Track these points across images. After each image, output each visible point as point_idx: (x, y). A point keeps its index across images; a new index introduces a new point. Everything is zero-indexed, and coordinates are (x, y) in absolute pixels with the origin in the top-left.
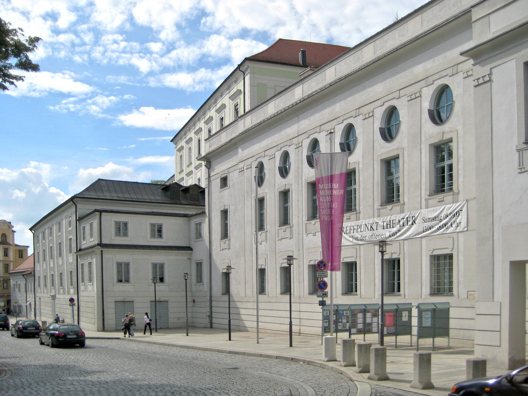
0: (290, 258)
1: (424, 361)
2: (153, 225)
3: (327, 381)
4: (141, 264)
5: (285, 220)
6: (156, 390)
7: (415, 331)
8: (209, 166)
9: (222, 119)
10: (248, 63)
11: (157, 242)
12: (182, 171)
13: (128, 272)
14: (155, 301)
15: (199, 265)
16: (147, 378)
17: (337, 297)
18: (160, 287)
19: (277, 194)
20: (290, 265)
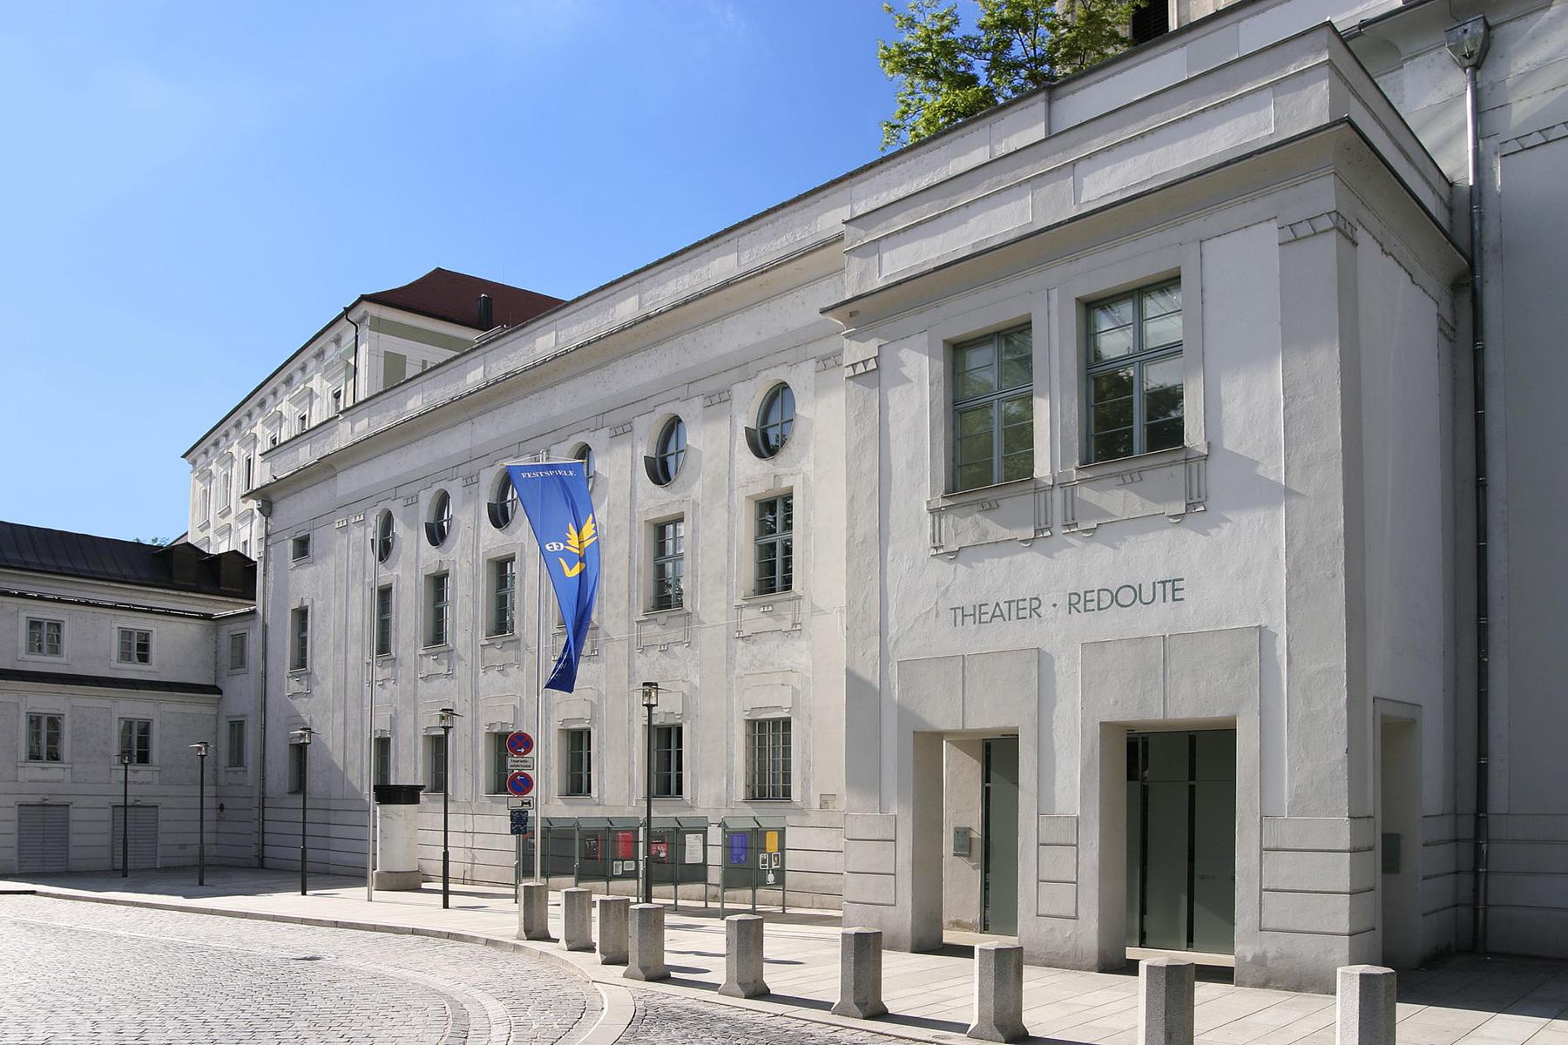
0: (448, 713)
1: (748, 938)
2: (126, 634)
3: (532, 983)
4: (94, 720)
5: (437, 635)
6: (95, 1017)
7: (715, 875)
8: (267, 509)
9: (303, 418)
10: (367, 307)
11: (134, 671)
12: (206, 525)
13: (54, 738)
14: (126, 806)
15: (237, 727)
16: (78, 986)
17: (549, 802)
18: (140, 773)
19: (422, 579)
20: (446, 729)
